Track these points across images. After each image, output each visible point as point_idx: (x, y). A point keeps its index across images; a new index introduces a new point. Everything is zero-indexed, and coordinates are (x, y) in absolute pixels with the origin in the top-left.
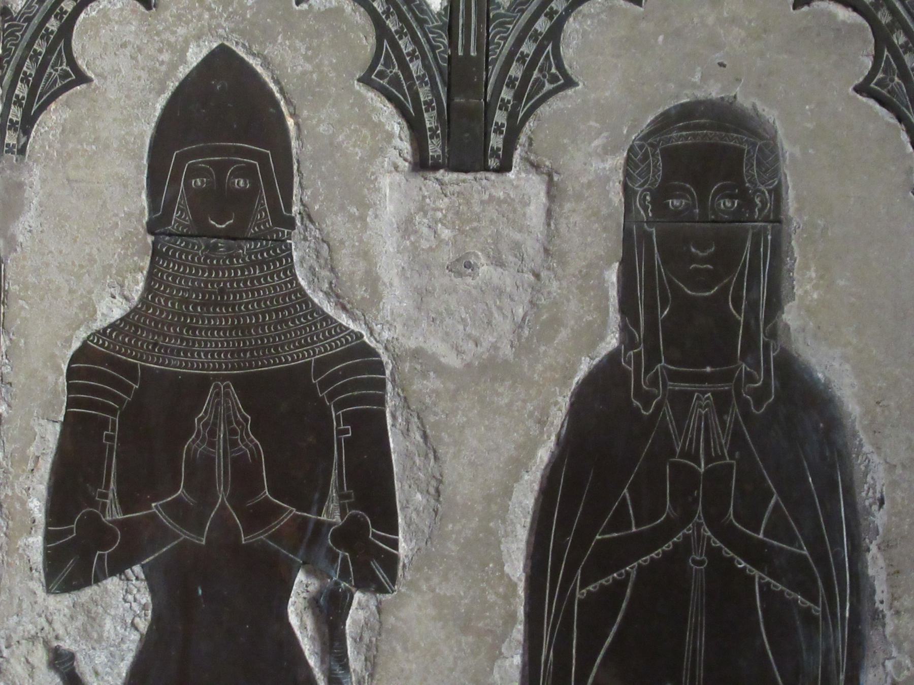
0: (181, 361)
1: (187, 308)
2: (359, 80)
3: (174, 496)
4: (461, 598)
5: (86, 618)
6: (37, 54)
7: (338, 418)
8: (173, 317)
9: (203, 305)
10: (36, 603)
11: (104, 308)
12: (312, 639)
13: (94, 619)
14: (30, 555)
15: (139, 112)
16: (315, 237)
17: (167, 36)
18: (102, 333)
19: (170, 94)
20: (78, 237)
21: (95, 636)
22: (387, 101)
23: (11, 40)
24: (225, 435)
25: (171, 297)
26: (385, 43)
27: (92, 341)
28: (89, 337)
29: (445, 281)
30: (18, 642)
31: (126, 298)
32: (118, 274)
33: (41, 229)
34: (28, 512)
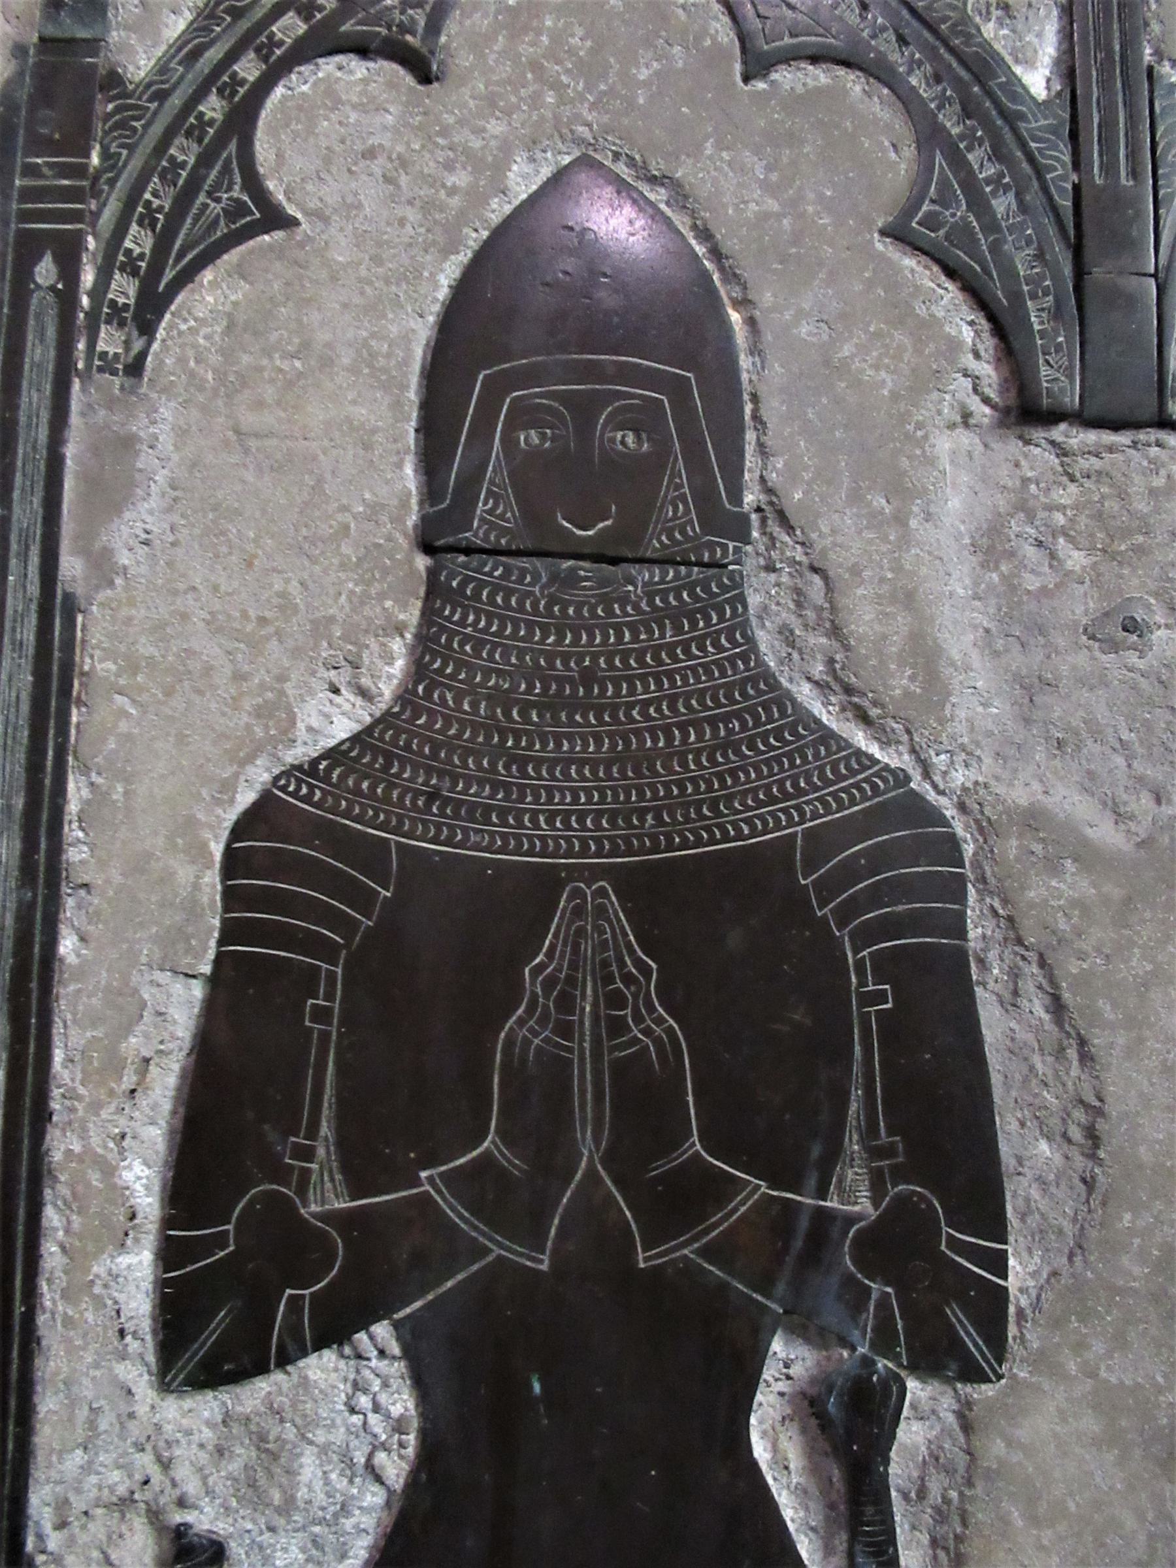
0: (492, 834)
1: (507, 714)
2: (883, 233)
3: (475, 1153)
4: (1160, 1390)
5: (254, 1454)
6: (176, 165)
7: (860, 966)
8: (474, 735)
9: (541, 707)
10: (132, 1416)
11: (314, 713)
12: (801, 1492)
13: (275, 1456)
14: (121, 1298)
15: (401, 290)
16: (793, 562)
17: (461, 136)
18: (310, 769)
19: (470, 255)
20: (255, 556)
21: (277, 1497)
22: (943, 278)
23: (121, 136)
24: (595, 1005)
25: (472, 689)
26: (938, 158)
27: (283, 789)
28: (276, 779)
29: (1081, 659)
30: (86, 1513)
31: (363, 693)
32: (345, 638)
33: (171, 539)
34: (118, 1193)
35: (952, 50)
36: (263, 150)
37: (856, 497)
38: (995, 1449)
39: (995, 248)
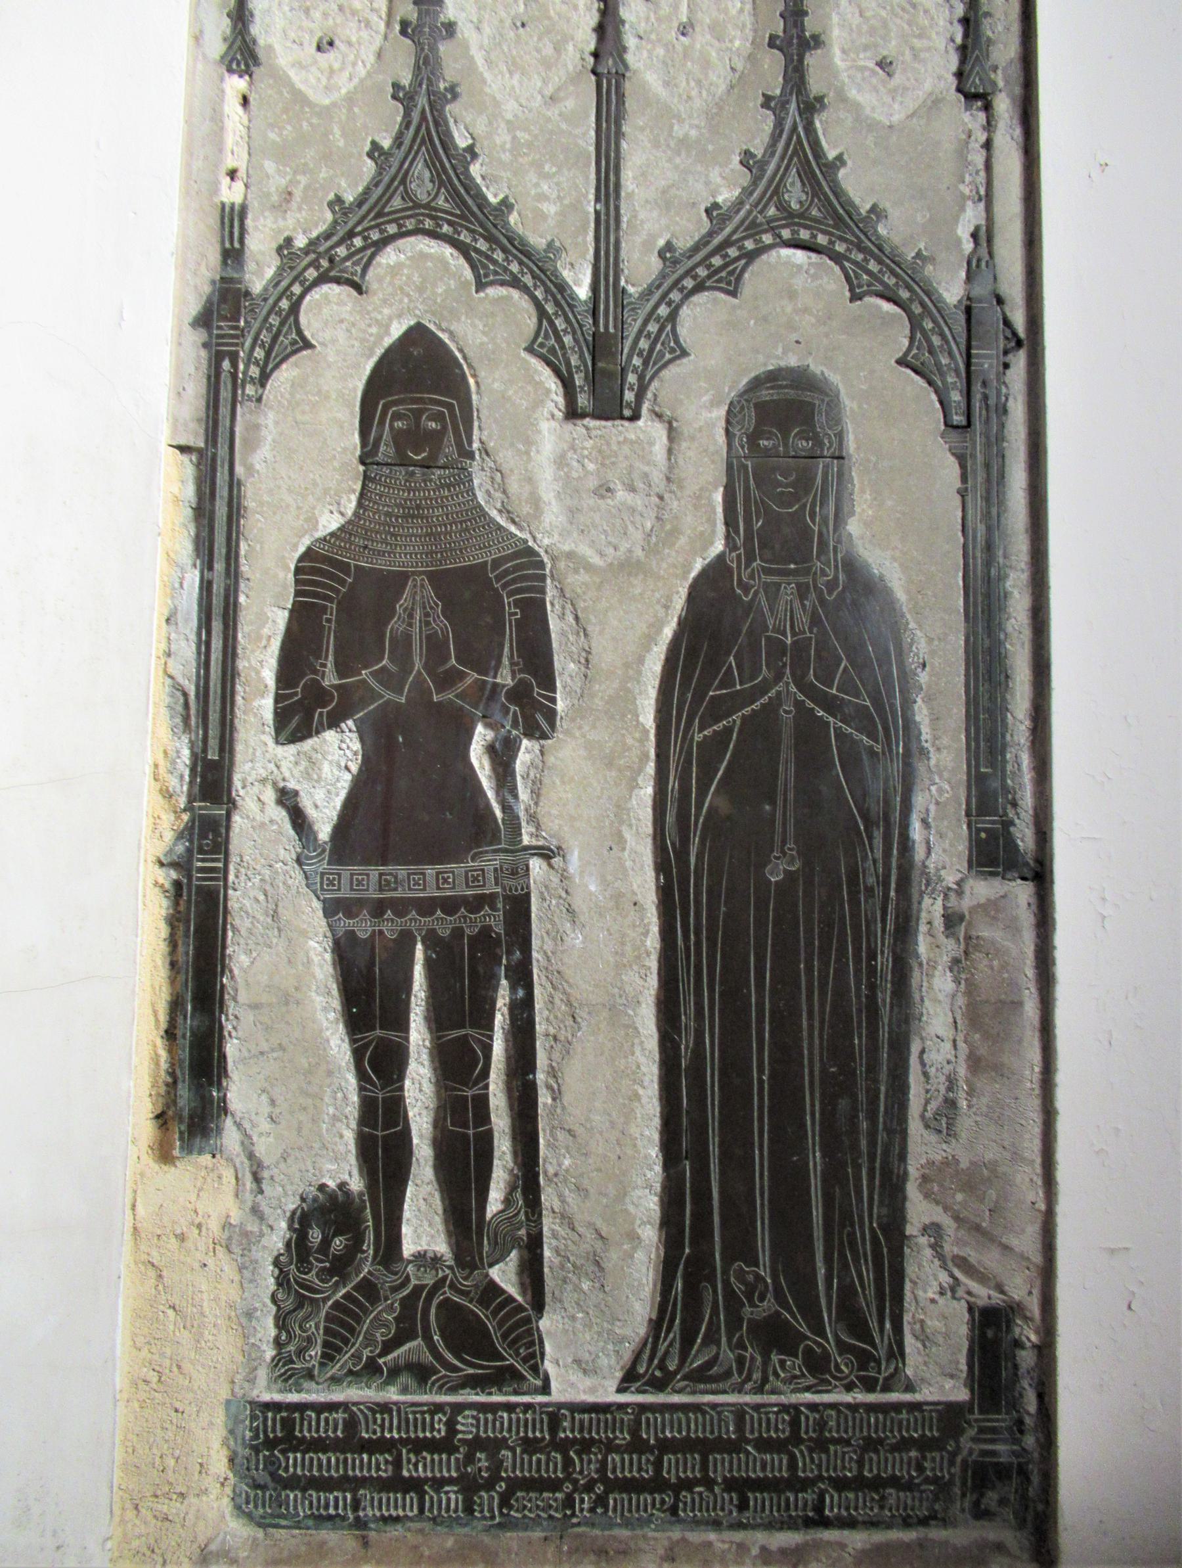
7: (509, 603)
17: (375, 315)
29: (591, 502)
31: (342, 514)
34: (261, 680)
35: (551, 281)
36: (303, 320)
37: (512, 445)
38: (551, 760)
39: (564, 355)
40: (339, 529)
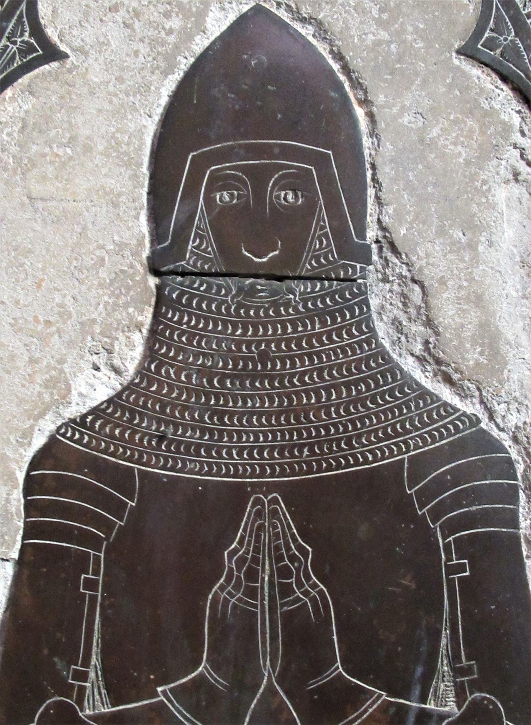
7: (447, 547)
31: (116, 371)
37: (442, 232)
40: (110, 401)
